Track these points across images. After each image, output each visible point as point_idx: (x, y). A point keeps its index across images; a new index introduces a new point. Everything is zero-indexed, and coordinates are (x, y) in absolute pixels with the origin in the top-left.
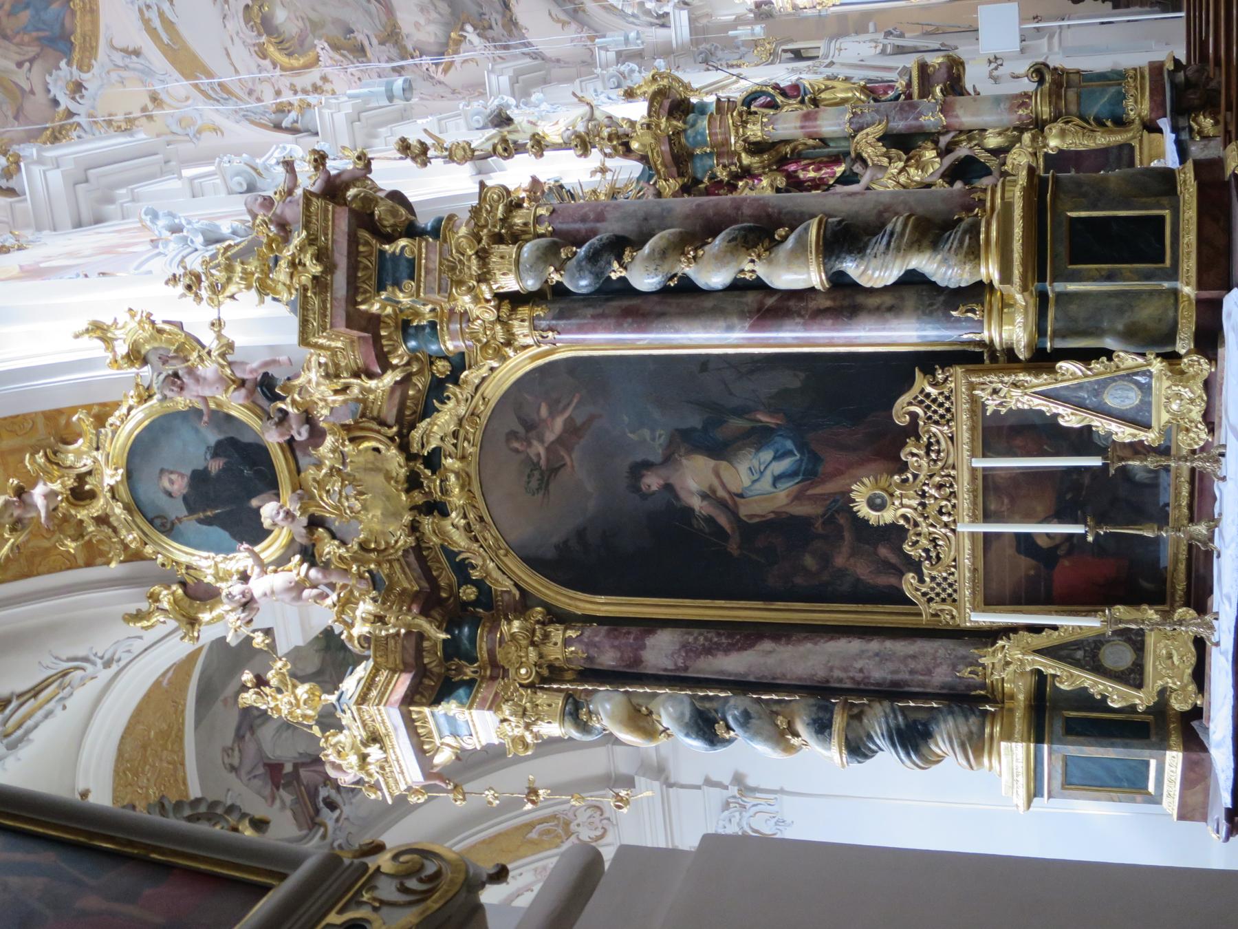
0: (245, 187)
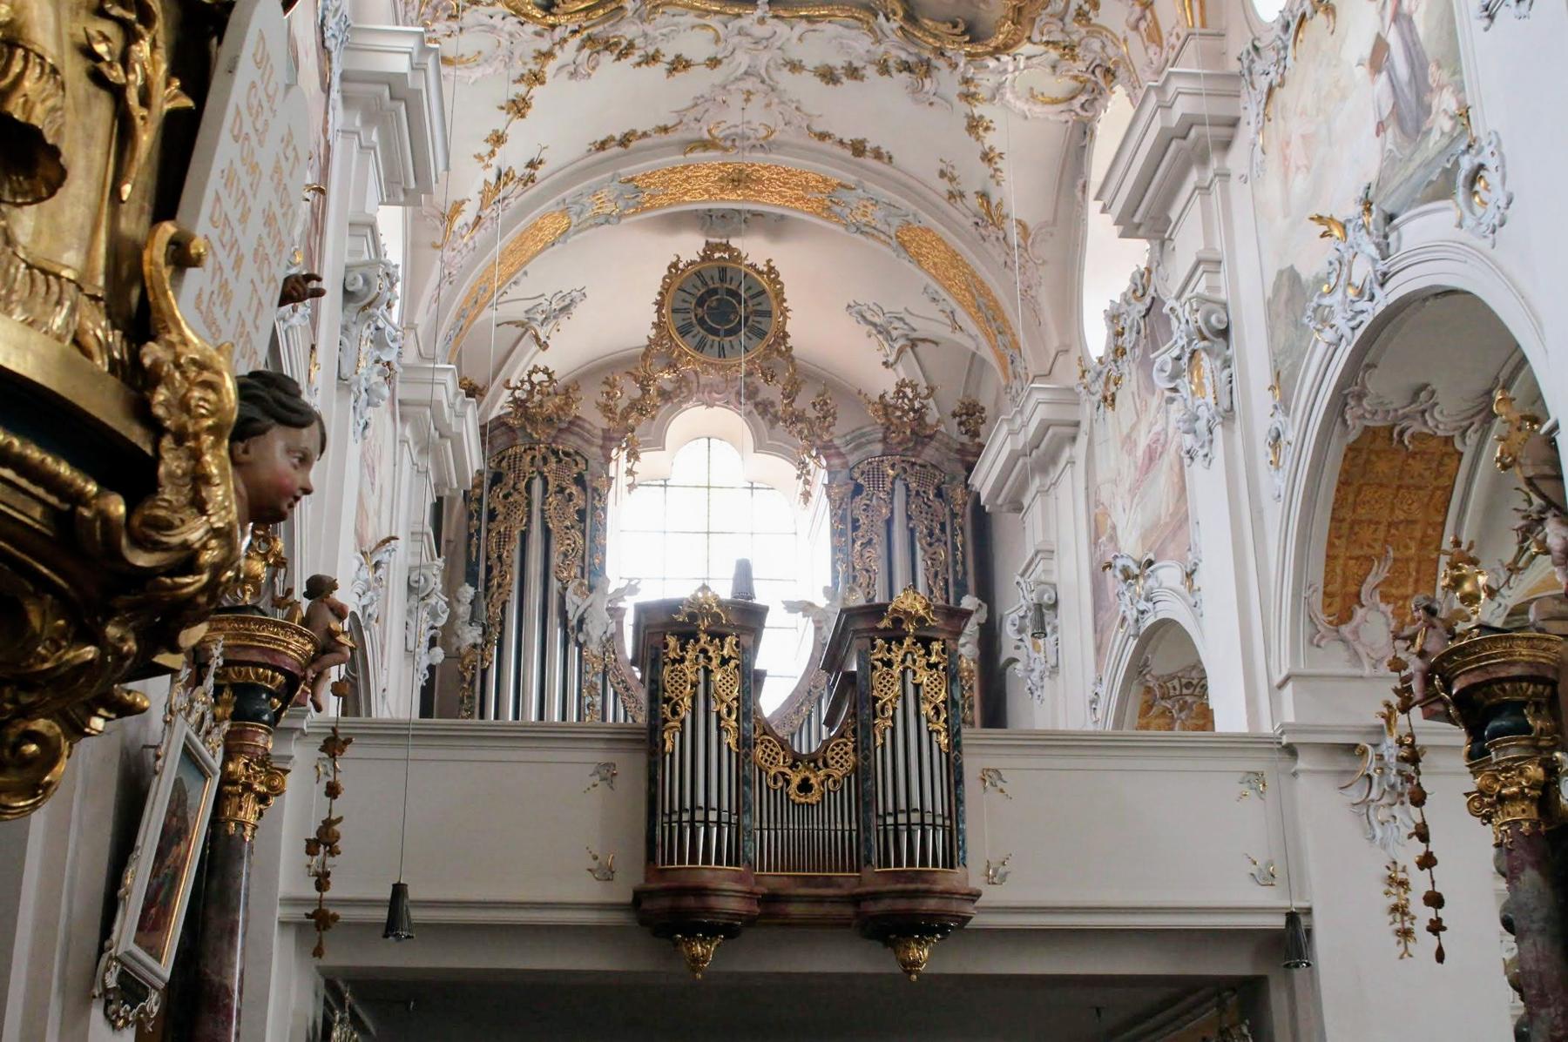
0: (350, 288)
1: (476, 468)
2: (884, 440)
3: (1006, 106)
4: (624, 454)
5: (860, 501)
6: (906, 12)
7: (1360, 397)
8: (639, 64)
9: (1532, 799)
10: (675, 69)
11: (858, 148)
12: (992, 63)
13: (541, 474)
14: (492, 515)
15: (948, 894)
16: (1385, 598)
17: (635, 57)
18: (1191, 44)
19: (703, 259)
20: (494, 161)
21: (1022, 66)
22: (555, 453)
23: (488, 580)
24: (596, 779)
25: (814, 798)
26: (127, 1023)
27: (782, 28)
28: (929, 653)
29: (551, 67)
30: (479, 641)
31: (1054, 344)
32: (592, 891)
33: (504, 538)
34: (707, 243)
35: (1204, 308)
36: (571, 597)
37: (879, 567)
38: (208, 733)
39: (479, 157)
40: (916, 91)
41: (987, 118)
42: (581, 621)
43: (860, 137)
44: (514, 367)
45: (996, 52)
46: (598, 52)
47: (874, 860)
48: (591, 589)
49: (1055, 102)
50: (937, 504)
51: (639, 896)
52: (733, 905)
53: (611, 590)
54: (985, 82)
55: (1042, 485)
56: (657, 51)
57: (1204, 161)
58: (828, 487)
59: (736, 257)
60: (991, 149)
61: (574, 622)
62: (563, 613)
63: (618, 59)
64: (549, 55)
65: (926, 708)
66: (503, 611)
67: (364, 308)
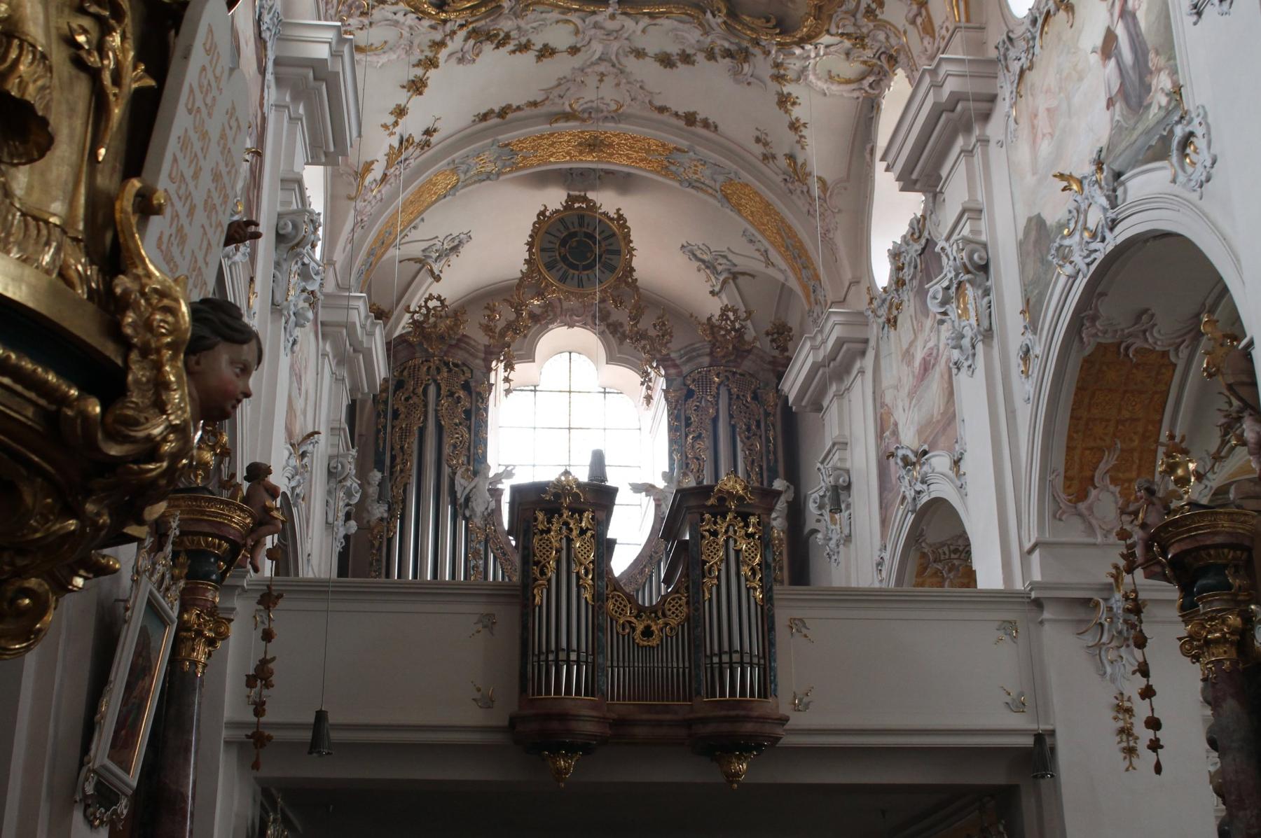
0: (281, 232)
1: (383, 375)
2: (711, 354)
3: (809, 85)
4: (502, 366)
5: (692, 403)
6: (728, 9)
7: (1093, 319)
8: (514, 52)
9: (1232, 643)
10: (543, 56)
11: (690, 119)
12: (798, 51)
13: (435, 381)
14: (396, 414)
15: (763, 719)
16: (1114, 481)
17: (510, 47)
18: (958, 35)
19: (565, 208)
20: (398, 130)
21: (822, 53)
22: (447, 364)
23: (393, 466)
24: (480, 626)
25: (654, 641)
26: (102, 822)
27: (629, 23)
28: (747, 525)
29: (443, 54)
30: (386, 515)
31: (848, 276)
32: (473, 716)
33: (405, 433)
34: (569, 196)
35: (968, 248)
36: (459, 480)
37: (706, 456)
38: (167, 589)
39: (385, 126)
40: (736, 74)
41: (794, 95)
42: (468, 499)
43: (692, 110)
44: (411, 299)
45: (801, 42)
46: (481, 42)
47: (703, 692)
48: (475, 473)
49: (848, 82)
50: (753, 406)
51: (513, 721)
52: (590, 728)
53: (491, 474)
54: (792, 66)
55: (837, 390)
56: (529, 41)
57: (968, 130)
58: (666, 392)
59: (592, 207)
60: (797, 120)
61: (462, 500)
62: (453, 493)
63: (497, 47)
64: (441, 44)
65: (745, 570)
66: (405, 491)
67: (293, 248)
